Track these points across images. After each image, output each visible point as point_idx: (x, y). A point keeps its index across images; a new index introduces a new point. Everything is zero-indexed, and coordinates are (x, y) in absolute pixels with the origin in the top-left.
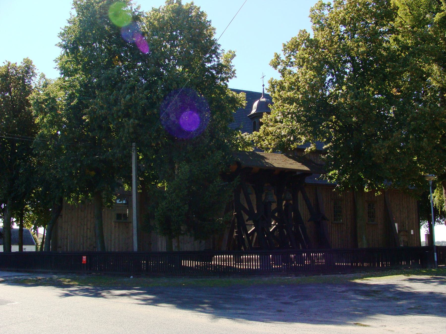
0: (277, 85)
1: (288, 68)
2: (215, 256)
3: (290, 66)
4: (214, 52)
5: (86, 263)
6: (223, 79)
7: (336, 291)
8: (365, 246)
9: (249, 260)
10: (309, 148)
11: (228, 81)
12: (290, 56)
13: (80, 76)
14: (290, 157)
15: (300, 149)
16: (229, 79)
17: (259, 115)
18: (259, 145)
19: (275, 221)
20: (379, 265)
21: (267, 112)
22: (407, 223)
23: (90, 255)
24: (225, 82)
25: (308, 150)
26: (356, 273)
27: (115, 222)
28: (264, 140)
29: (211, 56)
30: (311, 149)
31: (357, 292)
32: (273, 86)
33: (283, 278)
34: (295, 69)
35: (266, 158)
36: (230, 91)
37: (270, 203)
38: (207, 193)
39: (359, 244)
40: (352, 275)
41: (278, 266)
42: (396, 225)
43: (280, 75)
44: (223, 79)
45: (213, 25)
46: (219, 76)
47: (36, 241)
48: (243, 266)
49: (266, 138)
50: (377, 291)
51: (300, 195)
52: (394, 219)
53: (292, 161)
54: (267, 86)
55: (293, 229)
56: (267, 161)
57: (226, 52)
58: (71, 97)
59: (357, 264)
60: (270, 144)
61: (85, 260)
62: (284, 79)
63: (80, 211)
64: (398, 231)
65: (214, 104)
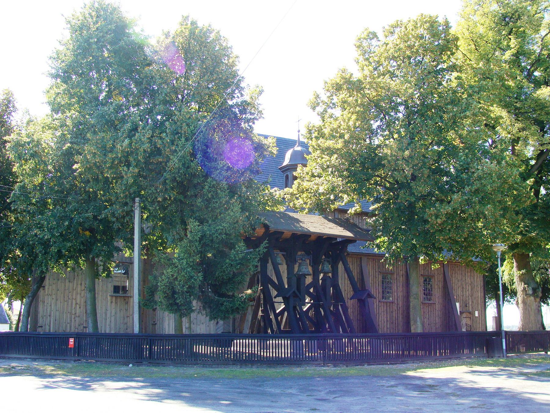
0: (316, 131)
1: (330, 111)
2: (235, 341)
3: (332, 108)
4: (238, 86)
5: (73, 347)
6: (248, 121)
7: (383, 386)
8: (419, 330)
9: (277, 346)
10: (354, 209)
11: (254, 123)
12: (332, 96)
13: (73, 113)
14: (329, 220)
15: (343, 211)
16: (255, 121)
17: (292, 167)
18: (291, 205)
19: (310, 299)
20: (435, 354)
21: (302, 164)
22: (470, 303)
23: (78, 337)
24: (250, 124)
25: (352, 211)
26: (407, 363)
27: (112, 296)
28: (297, 199)
29: (233, 92)
30: (355, 211)
31: (410, 386)
32: (310, 132)
33: (318, 368)
34: (337, 112)
35: (301, 222)
36: (257, 136)
37: (304, 276)
38: (227, 261)
39: (412, 328)
40: (404, 365)
41: (313, 354)
42: (458, 304)
43: (319, 118)
44: (248, 121)
45: (235, 51)
46: (244, 116)
47: (10, 319)
48: (264, 354)
49: (300, 196)
50: (433, 386)
51: (341, 266)
52: (455, 297)
53: (332, 225)
54: (304, 131)
55: (332, 309)
56: (301, 224)
57: (253, 87)
58: (62, 139)
59: (409, 353)
60: (306, 203)
61: (72, 343)
62: (323, 124)
63: (67, 281)
64: (460, 312)
65: (235, 152)
